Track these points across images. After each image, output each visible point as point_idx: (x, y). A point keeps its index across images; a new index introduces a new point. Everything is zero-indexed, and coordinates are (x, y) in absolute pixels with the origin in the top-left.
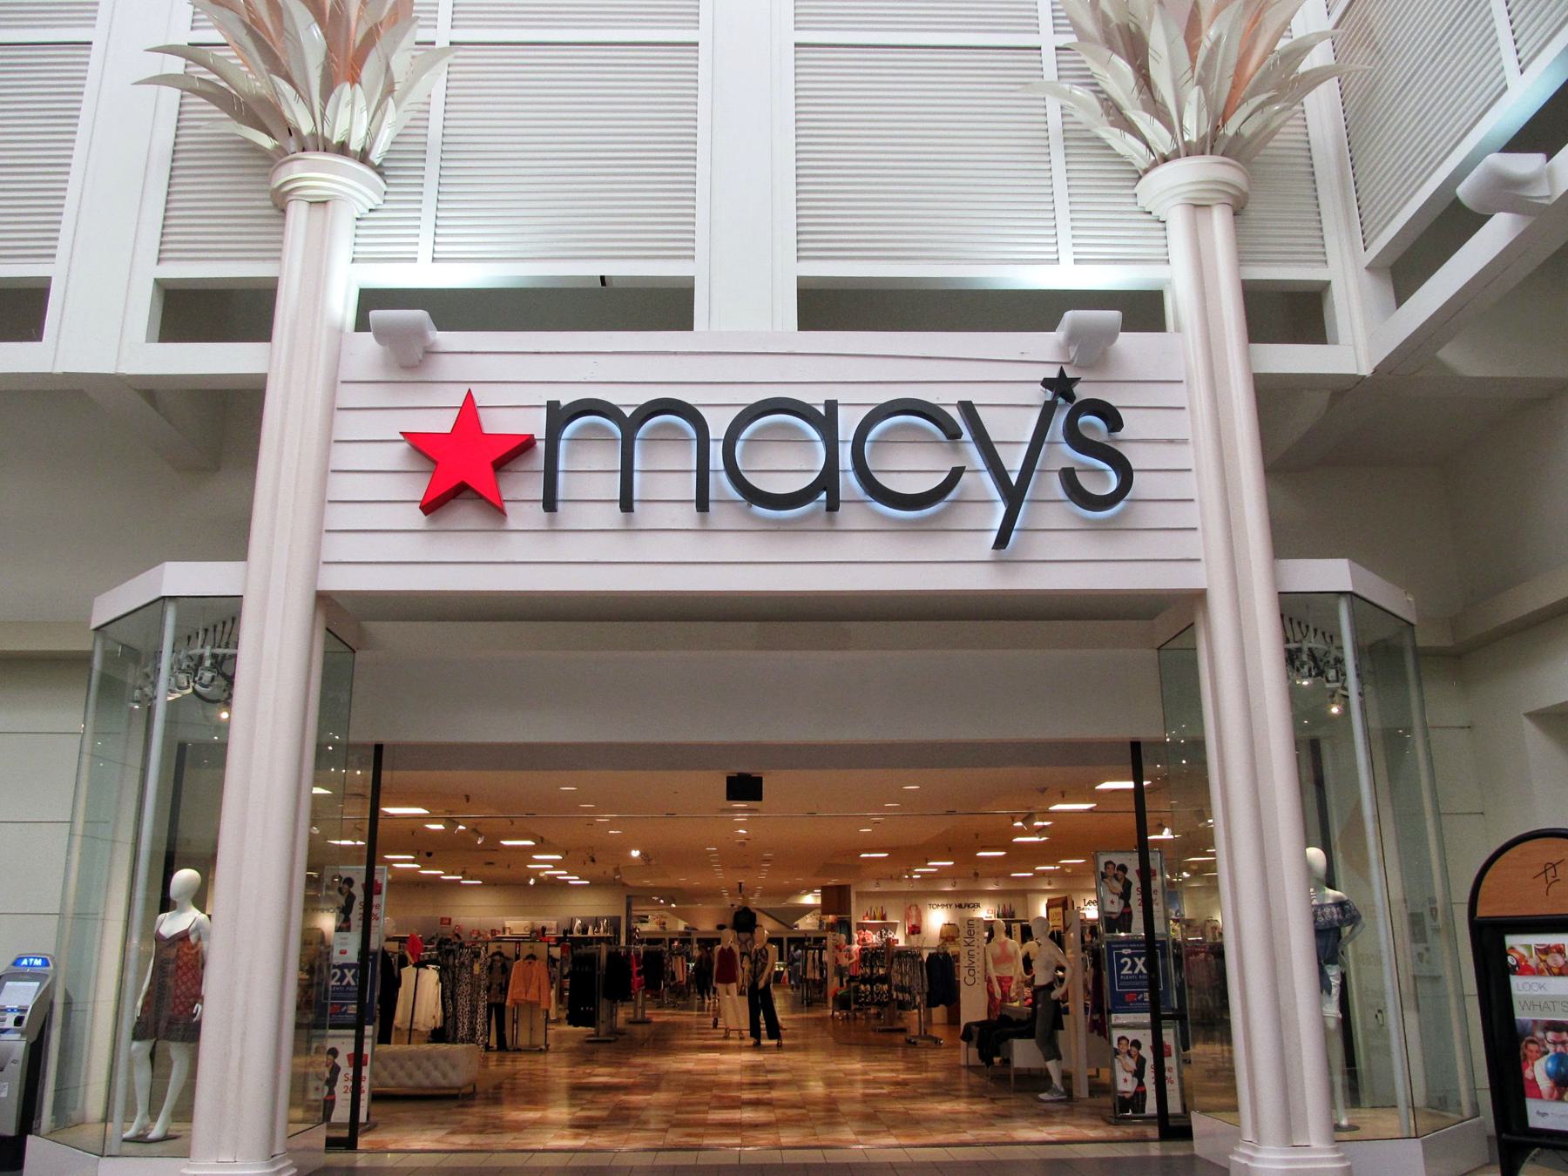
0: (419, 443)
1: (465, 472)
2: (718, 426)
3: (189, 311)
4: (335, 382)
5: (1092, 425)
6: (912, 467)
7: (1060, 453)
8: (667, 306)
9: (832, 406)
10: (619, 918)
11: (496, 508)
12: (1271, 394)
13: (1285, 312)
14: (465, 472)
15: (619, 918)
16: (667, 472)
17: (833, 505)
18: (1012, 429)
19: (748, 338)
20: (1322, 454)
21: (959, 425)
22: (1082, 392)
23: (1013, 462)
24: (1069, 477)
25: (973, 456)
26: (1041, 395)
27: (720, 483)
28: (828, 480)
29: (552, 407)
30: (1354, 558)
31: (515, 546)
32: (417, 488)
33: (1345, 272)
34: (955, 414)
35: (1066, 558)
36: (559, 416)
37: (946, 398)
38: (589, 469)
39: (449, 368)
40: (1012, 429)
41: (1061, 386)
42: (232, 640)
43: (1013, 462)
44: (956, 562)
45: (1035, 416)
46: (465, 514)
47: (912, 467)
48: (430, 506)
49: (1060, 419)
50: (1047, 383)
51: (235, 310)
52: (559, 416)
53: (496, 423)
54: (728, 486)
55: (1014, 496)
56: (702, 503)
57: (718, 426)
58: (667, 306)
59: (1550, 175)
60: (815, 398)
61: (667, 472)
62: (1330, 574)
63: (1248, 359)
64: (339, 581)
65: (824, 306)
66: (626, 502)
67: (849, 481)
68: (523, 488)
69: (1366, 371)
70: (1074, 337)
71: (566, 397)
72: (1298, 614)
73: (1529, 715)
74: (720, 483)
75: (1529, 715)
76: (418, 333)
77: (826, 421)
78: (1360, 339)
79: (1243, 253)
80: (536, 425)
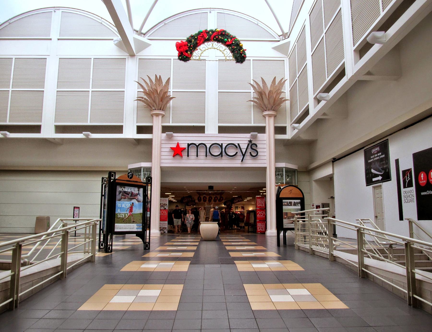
0: (172, 148)
1: (177, 151)
2: (208, 147)
3: (140, 130)
4: (161, 140)
5: (254, 147)
6: (231, 152)
7: (249, 150)
8: (201, 130)
9: (222, 144)
10: (373, 187)
11: (181, 156)
12: (277, 141)
13: (281, 130)
14: (177, 151)
15: (373, 187)
16: (202, 152)
17: (222, 156)
18: (244, 147)
19: (211, 135)
20: (284, 147)
21: (238, 147)
22: (253, 142)
23: (244, 151)
24: (250, 153)
25: (239, 151)
26: (247, 142)
27: (208, 153)
28: (221, 153)
29: (188, 144)
30: (286, 162)
31: (183, 161)
32: (172, 153)
33: (288, 125)
34: (237, 145)
35: (249, 163)
36: (189, 145)
37: (236, 143)
38: (193, 151)
39: (175, 138)
40: (244, 147)
41: (250, 141)
42: (151, 172)
43: (244, 151)
44: (237, 163)
45: (247, 145)
46: (178, 157)
47: (231, 152)
48: (174, 156)
49: (249, 147)
50: (249, 141)
51: (148, 130)
52: (189, 145)
53: (182, 146)
54: (208, 153)
55: (244, 155)
56: (206, 156)
57: (208, 147)
58: (201, 130)
59: (329, 96)
60: (220, 143)
61: (202, 152)
62: (282, 165)
63: (274, 137)
64: (163, 165)
65: (222, 130)
66: (197, 156)
67: (224, 153)
68: (185, 154)
69: (290, 138)
70: (252, 135)
71: (190, 142)
72: (278, 171)
73: (314, 181)
74: (208, 153)
75: (314, 181)
76: (172, 135)
77: (221, 146)
78: (289, 135)
79: (274, 123)
80: (186, 146)
